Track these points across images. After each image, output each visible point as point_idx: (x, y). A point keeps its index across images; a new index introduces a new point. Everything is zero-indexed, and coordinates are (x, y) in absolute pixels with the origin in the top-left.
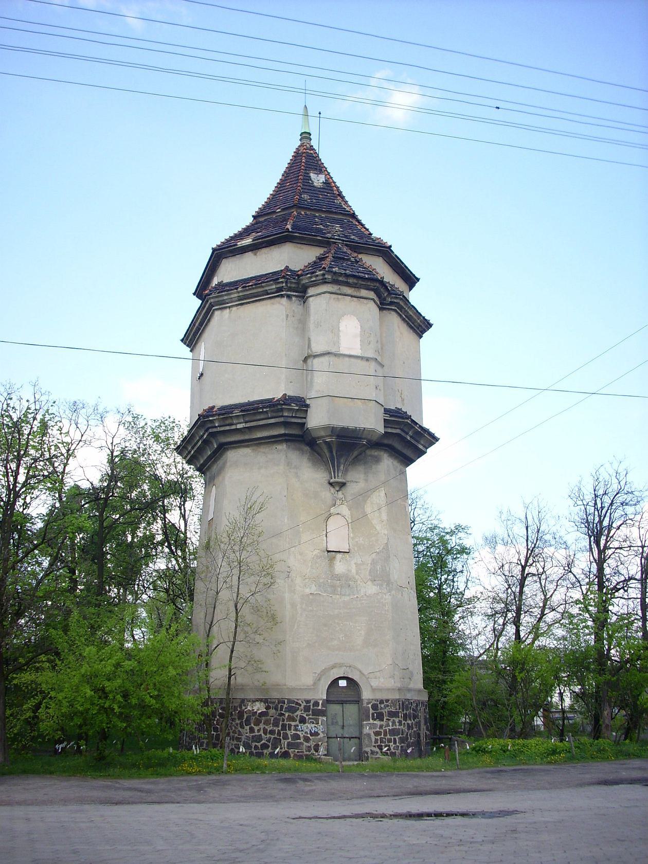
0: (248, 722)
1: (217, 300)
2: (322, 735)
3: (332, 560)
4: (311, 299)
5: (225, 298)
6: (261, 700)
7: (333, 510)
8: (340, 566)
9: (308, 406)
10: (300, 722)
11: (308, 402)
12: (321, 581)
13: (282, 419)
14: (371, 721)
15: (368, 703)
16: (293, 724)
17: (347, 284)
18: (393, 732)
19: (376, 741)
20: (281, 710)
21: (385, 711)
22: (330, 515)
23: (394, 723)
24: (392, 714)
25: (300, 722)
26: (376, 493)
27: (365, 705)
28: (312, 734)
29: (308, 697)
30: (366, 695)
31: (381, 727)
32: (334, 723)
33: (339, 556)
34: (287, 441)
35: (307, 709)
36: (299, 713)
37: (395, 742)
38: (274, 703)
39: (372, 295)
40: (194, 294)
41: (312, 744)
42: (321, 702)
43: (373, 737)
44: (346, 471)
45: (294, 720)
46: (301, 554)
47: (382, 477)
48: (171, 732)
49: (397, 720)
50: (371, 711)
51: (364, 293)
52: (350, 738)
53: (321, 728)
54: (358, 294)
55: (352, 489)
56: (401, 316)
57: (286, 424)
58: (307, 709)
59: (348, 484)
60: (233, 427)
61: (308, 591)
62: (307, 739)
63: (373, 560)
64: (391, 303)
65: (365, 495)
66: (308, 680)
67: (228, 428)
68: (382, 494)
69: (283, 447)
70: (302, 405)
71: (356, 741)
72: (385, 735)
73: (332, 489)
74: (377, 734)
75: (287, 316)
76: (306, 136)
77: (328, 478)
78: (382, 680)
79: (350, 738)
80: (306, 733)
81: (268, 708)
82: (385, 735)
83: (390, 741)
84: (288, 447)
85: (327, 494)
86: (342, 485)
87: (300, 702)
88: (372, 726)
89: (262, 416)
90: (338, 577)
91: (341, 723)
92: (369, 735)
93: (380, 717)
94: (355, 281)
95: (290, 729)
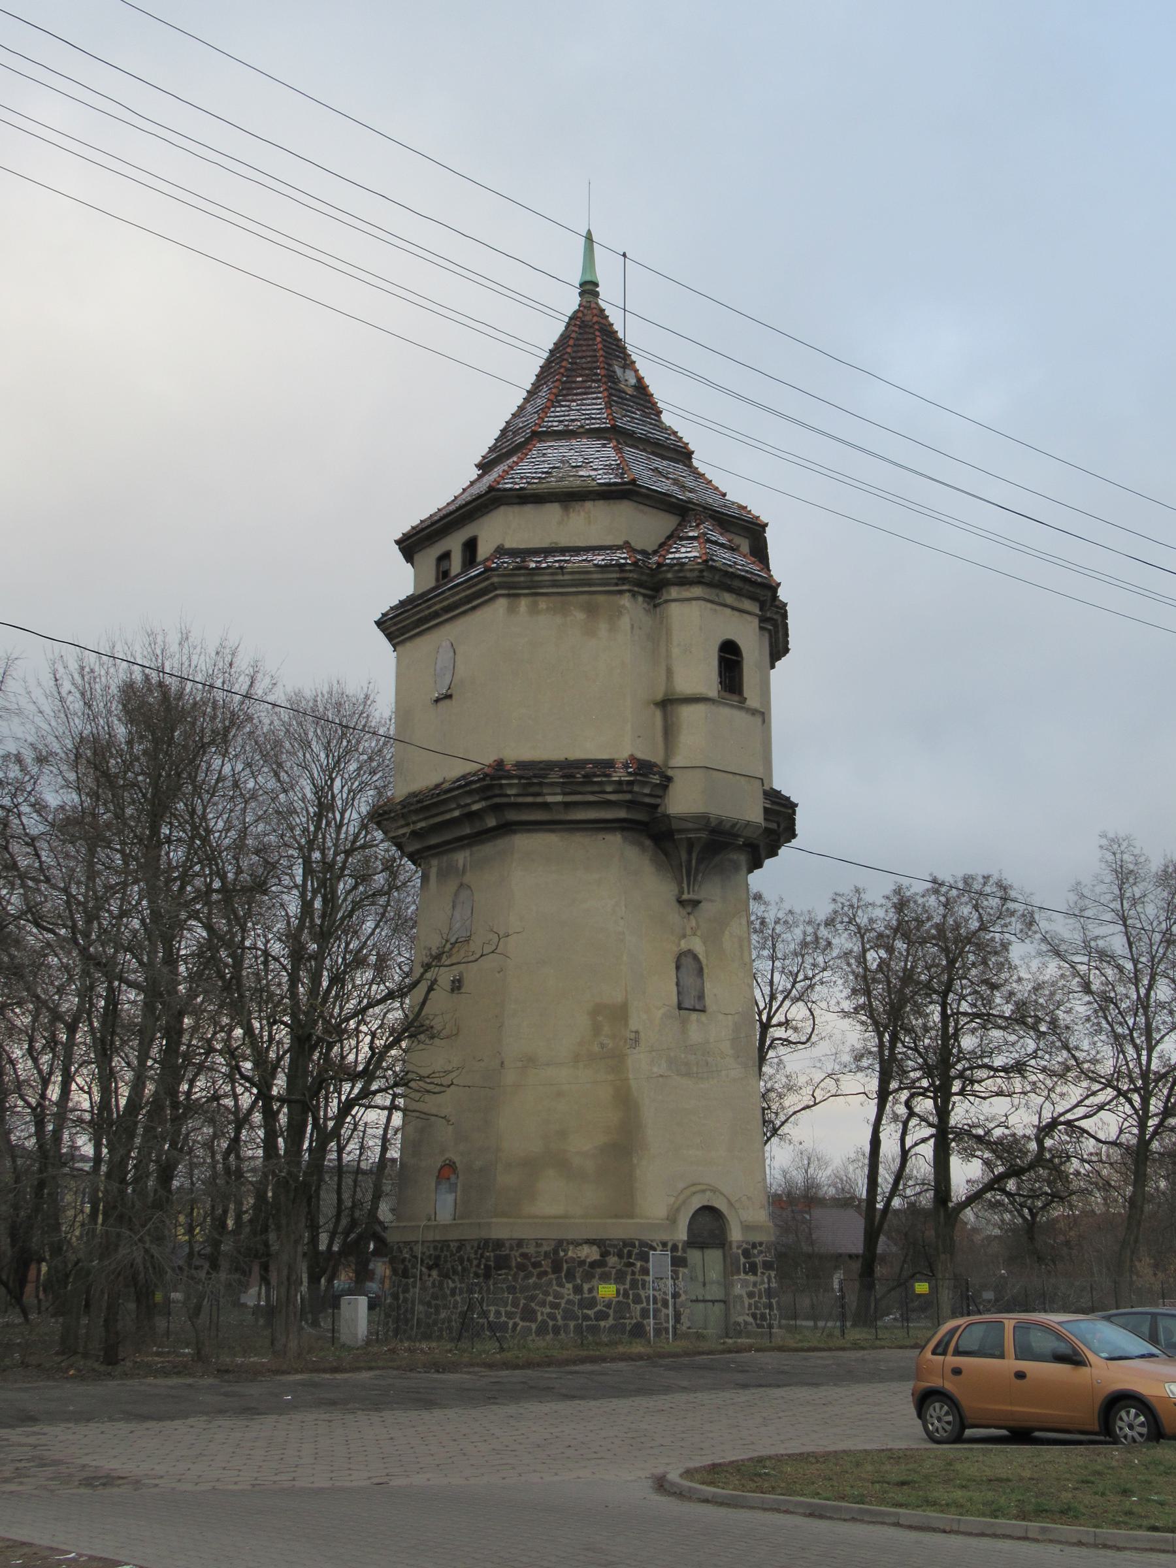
0: (570, 1276)
1: (505, 579)
4: (673, 605)
6: (590, 1242)
9: (669, 779)
11: (670, 773)
13: (628, 797)
17: (730, 589)
19: (750, 1305)
20: (629, 1256)
21: (759, 1260)
24: (767, 1266)
27: (735, 1250)
30: (736, 1235)
31: (755, 1284)
34: (623, 829)
38: (615, 1246)
39: (754, 607)
40: (398, 542)
42: (680, 1246)
43: (746, 1301)
48: (464, 1297)
51: (748, 605)
52: (713, 1302)
55: (709, 909)
57: (631, 805)
60: (539, 800)
67: (530, 799)
69: (615, 840)
71: (722, 1305)
72: (760, 1298)
74: (751, 1295)
75: (632, 627)
76: (589, 289)
77: (676, 892)
81: (604, 1254)
82: (760, 1298)
84: (625, 839)
86: (696, 903)
87: (654, 1244)
88: (745, 1283)
89: (596, 788)
91: (701, 1279)
92: (741, 1297)
93: (753, 1269)
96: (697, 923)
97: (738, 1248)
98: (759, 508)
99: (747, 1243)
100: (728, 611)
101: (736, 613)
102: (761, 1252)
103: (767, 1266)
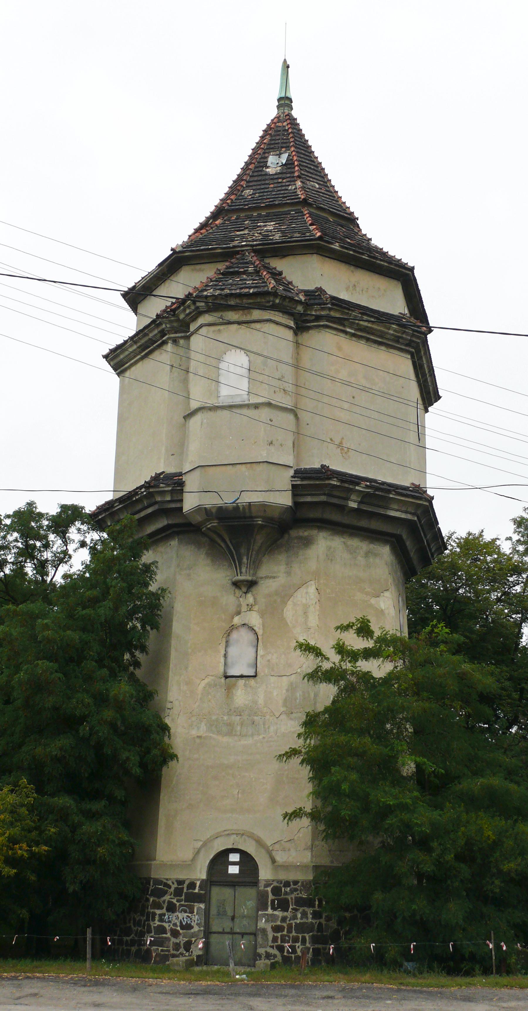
2: (196, 929)
3: (229, 689)
5: (122, 357)
7: (237, 620)
8: (241, 696)
10: (168, 910)
12: (214, 718)
13: (156, 507)
14: (270, 911)
15: (267, 886)
16: (158, 912)
18: (301, 928)
19: (275, 939)
21: (291, 897)
22: (233, 628)
23: (304, 914)
24: (300, 902)
25: (168, 910)
26: (302, 590)
27: (262, 888)
28: (182, 927)
29: (181, 877)
30: (265, 873)
31: (284, 919)
32: (221, 914)
33: (241, 682)
34: (178, 533)
35: (178, 892)
36: (167, 898)
37: (304, 941)
41: (182, 940)
42: (198, 883)
44: (256, 564)
45: (160, 907)
46: (187, 684)
47: (312, 565)
49: (310, 911)
50: (271, 897)
51: (257, 314)
52: (243, 934)
53: (196, 919)
54: (248, 318)
55: (266, 587)
56: (346, 333)
58: (178, 892)
59: (261, 582)
61: (194, 732)
62: (175, 934)
63: (291, 684)
64: (318, 318)
65: (285, 595)
66: (186, 854)
68: (312, 589)
70: (174, 483)
72: (289, 931)
73: (237, 591)
74: (277, 929)
76: (285, 102)
78: (293, 853)
79: (243, 934)
80: (175, 925)
82: (289, 931)
83: (296, 940)
85: (230, 599)
86: (251, 585)
87: (170, 882)
90: (239, 712)
92: (264, 931)
93: (283, 905)
94: (238, 301)
95: (154, 920)
96: (255, 599)
97: (267, 886)
98: (407, 259)
99: (280, 882)
100: (235, 326)
101: (243, 327)
102: (296, 890)
103: (300, 902)
